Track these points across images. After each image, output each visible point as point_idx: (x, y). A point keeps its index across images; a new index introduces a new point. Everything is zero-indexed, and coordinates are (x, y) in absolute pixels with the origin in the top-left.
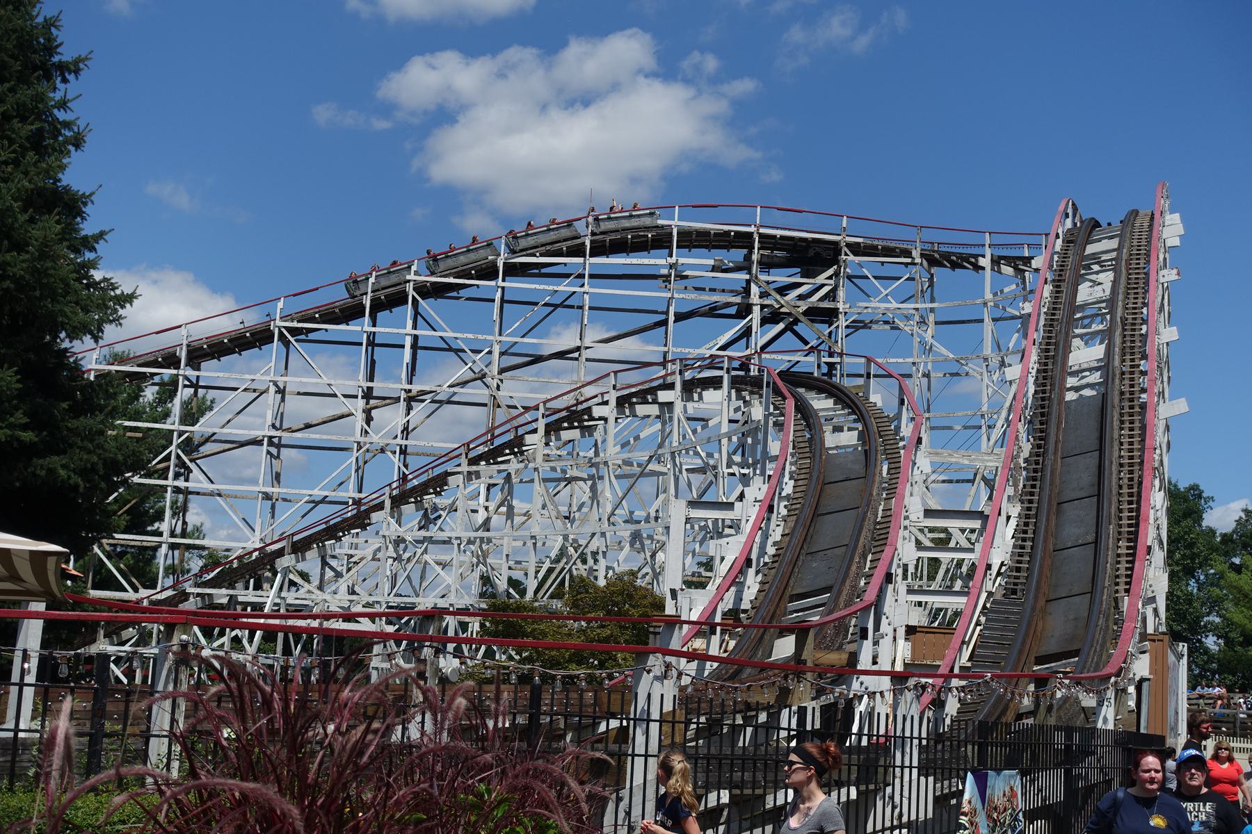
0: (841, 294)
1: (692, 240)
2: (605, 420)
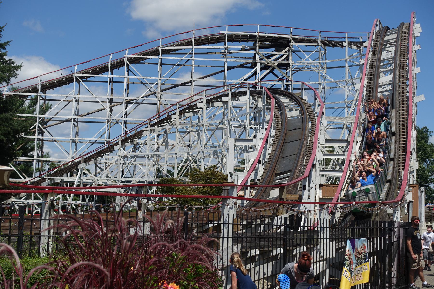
0: (291, 58)
1: (233, 39)
2: (202, 108)
